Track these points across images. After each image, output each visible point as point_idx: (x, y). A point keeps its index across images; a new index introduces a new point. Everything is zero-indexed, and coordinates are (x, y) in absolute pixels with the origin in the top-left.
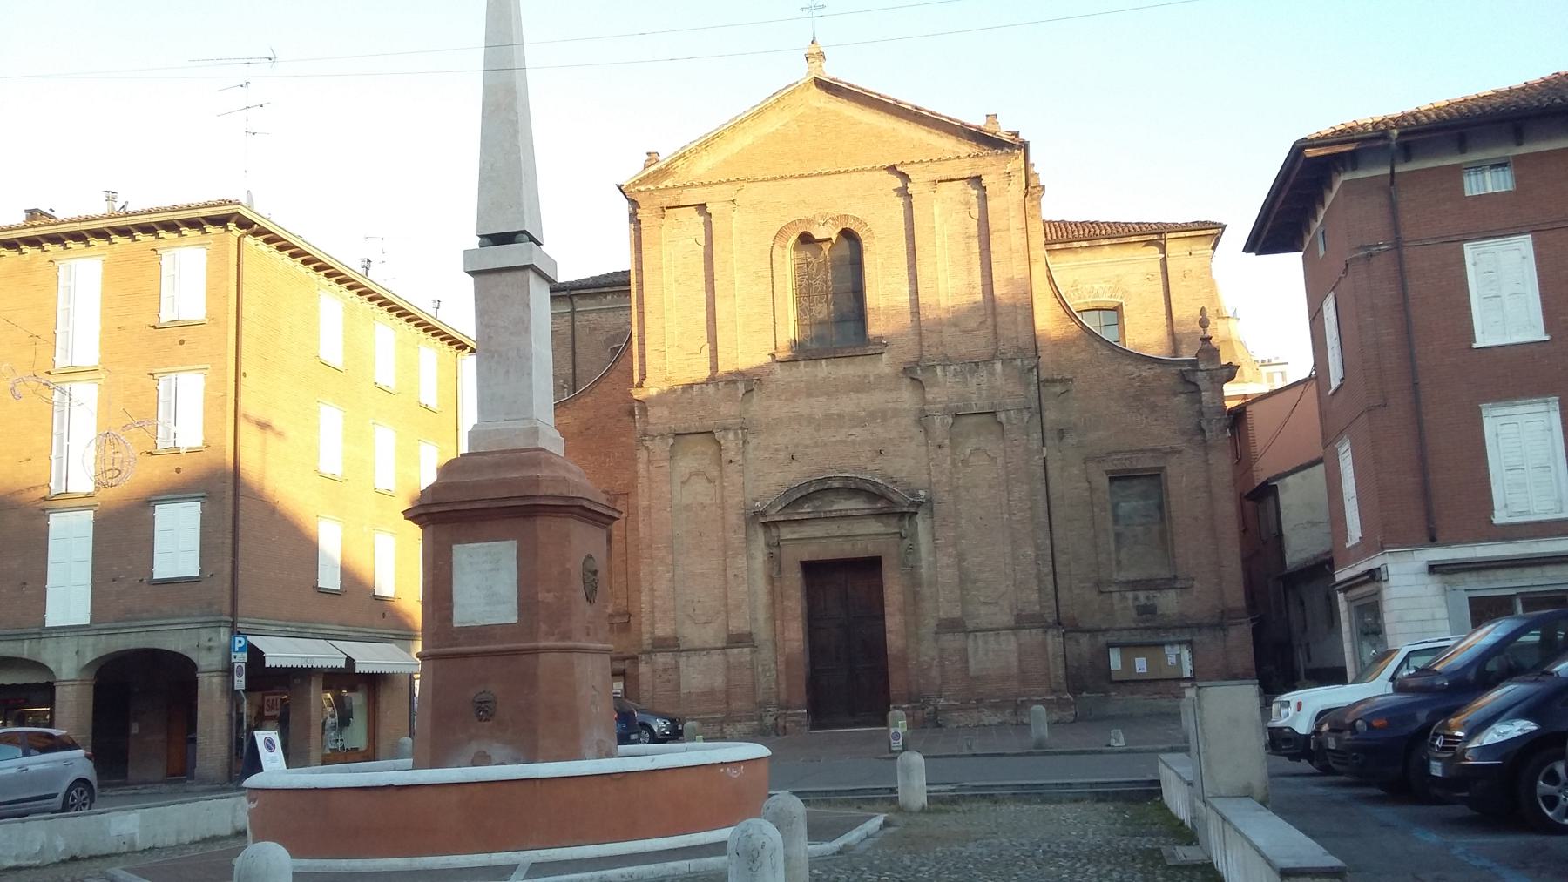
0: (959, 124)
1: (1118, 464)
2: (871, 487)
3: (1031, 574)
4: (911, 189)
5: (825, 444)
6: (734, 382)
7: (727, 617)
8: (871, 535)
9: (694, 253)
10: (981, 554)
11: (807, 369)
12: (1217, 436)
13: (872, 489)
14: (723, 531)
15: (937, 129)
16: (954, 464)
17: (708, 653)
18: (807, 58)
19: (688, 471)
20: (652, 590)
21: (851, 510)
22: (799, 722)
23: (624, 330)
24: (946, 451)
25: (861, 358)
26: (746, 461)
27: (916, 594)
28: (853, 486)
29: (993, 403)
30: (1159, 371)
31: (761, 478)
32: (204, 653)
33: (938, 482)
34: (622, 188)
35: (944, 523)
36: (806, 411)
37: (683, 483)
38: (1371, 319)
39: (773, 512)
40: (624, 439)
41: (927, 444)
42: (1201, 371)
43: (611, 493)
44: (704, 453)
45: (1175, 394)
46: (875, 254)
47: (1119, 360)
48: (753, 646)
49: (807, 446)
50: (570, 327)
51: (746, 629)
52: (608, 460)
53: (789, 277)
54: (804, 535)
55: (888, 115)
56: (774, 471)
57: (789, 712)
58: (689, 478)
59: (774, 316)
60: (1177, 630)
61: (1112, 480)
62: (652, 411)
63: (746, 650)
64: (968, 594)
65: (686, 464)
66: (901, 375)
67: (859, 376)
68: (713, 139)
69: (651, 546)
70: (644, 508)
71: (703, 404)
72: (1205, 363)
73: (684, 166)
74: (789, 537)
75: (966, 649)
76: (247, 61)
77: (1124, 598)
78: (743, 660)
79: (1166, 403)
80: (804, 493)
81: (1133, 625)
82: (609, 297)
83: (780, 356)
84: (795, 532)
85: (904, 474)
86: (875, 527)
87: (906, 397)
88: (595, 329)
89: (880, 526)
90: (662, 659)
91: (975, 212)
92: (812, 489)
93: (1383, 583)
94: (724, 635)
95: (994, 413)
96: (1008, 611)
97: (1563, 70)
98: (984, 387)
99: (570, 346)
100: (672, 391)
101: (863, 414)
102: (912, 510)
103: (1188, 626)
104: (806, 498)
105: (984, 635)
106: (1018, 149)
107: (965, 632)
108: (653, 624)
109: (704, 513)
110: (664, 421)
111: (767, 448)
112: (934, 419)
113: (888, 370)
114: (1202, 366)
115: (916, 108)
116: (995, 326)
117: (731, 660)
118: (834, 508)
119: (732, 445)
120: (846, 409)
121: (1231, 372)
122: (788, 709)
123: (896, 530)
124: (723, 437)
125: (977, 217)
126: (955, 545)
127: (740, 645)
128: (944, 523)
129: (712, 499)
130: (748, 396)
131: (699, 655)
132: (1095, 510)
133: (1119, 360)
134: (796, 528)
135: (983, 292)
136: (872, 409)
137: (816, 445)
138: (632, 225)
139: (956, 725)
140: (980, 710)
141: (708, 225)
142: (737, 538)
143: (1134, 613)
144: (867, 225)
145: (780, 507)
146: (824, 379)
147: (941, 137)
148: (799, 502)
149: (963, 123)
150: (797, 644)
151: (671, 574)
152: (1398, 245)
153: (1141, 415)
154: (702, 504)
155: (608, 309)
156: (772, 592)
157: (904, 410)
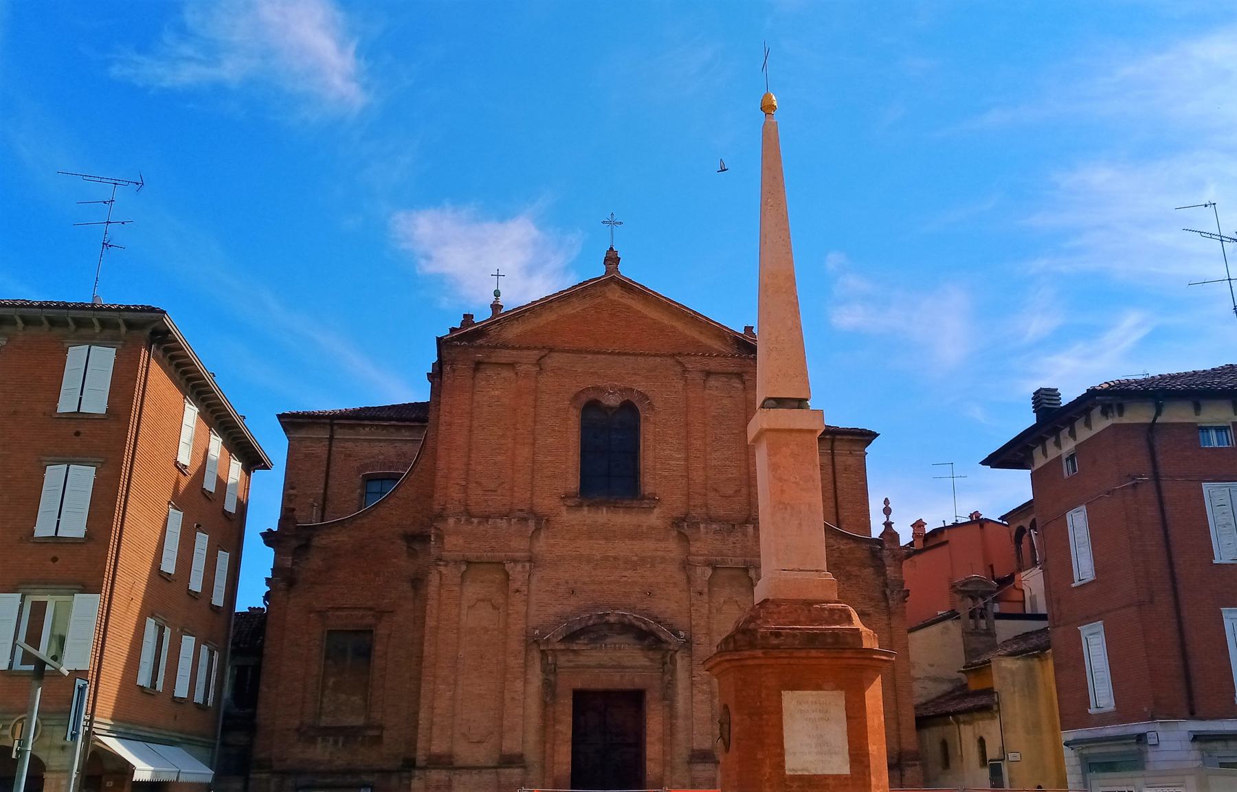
2: (643, 625)
11: (590, 515)
12: (898, 604)
20: (432, 708)
23: (377, 460)
24: (705, 597)
27: (672, 725)
32: (55, 753)
33: (697, 625)
38: (1139, 532)
40: (395, 560)
43: (377, 610)
48: (524, 767)
49: (584, 583)
50: (326, 452)
52: (377, 578)
58: (475, 604)
63: (517, 771)
65: (472, 591)
69: (435, 665)
70: (431, 628)
73: (497, 330)
76: (115, 182)
79: (859, 573)
82: (367, 429)
87: (673, 548)
88: (350, 456)
89: (646, 661)
90: (436, 776)
93: (1150, 749)
97: (1234, 363)
98: (739, 546)
99: (324, 469)
108: (430, 740)
109: (486, 637)
110: (458, 549)
113: (659, 523)
117: (503, 779)
120: (621, 554)
129: (495, 625)
142: (515, 663)
147: (711, 338)
150: (565, 767)
152: (1156, 477)
154: (485, 628)
155: (366, 439)
156: (544, 717)
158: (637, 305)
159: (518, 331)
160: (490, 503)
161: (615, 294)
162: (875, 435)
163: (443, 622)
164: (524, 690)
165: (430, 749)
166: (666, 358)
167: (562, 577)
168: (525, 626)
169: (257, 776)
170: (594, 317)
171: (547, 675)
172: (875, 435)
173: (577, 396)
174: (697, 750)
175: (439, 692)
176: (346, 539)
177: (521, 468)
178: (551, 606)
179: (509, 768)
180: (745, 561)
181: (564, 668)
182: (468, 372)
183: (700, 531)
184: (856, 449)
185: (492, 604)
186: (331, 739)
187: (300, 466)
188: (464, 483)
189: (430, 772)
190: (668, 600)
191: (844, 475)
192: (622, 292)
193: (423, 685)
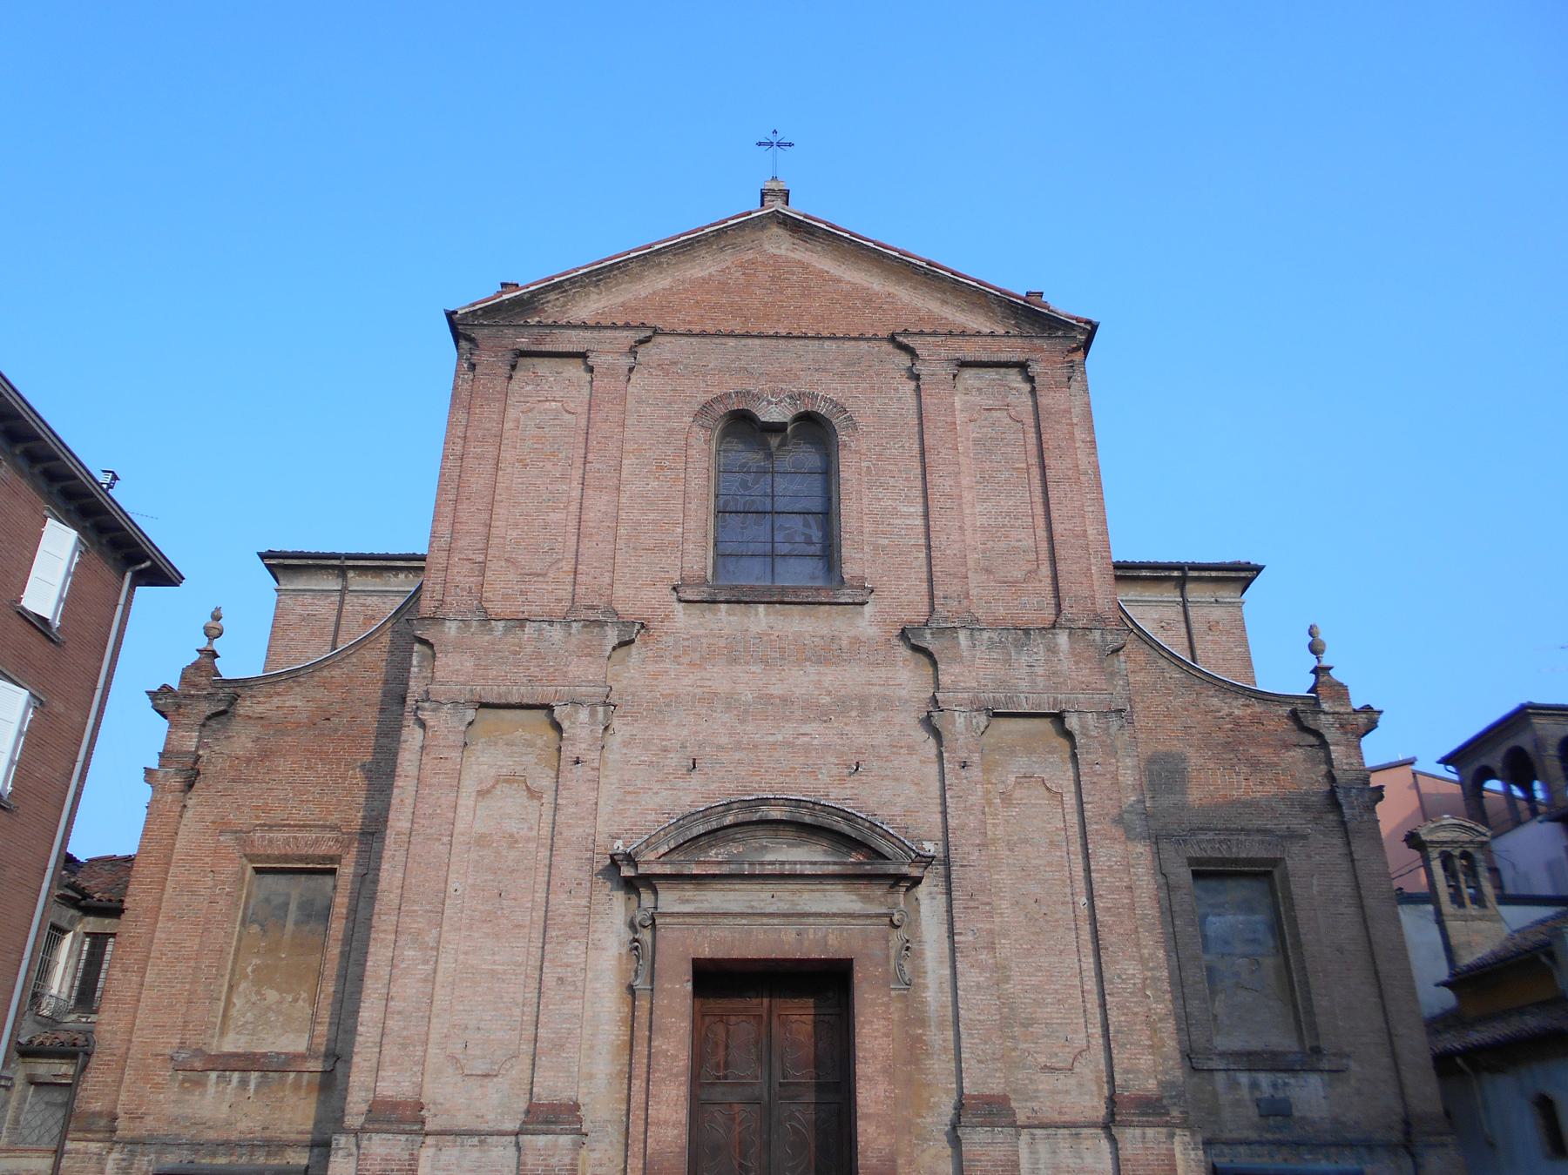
1: (1206, 848)
3: (1136, 1014)
5: (755, 746)
8: (834, 915)
9: (557, 422)
10: (1039, 968)
11: (731, 618)
13: (844, 827)
19: (493, 772)
21: (802, 863)
24: (975, 773)
28: (808, 819)
29: (1055, 699)
30: (1259, 710)
31: (629, 798)
33: (963, 827)
35: (972, 904)
36: (723, 686)
37: (482, 794)
42: (1326, 713)
44: (530, 744)
45: (1287, 746)
47: (1197, 688)
48: (579, 1132)
49: (720, 747)
51: (565, 1095)
54: (705, 907)
56: (656, 787)
58: (493, 787)
60: (1333, 1150)
61: (1196, 875)
62: (444, 660)
63: (565, 1140)
64: (1015, 1049)
65: (485, 762)
67: (823, 637)
72: (1330, 703)
74: (676, 909)
77: (1234, 1085)
80: (714, 825)
81: (1253, 1135)
84: (688, 901)
85: (896, 810)
86: (842, 899)
87: (907, 678)
90: (381, 1146)
92: (729, 820)
96: (1094, 1088)
98: (1040, 671)
99: (331, 638)
101: (826, 700)
102: (915, 872)
103: (1351, 1145)
104: (715, 835)
105: (1048, 1137)
107: (1013, 1124)
109: (513, 854)
110: (462, 679)
112: (953, 716)
113: (872, 631)
114: (1325, 706)
118: (769, 857)
119: (583, 733)
121: (1369, 718)
123: (883, 910)
128: (972, 904)
130: (622, 651)
132: (1177, 922)
133: (1197, 688)
134: (689, 891)
136: (843, 692)
137: (738, 746)
142: (567, 905)
143: (1252, 1112)
145: (665, 849)
147: (963, 310)
148: (703, 841)
153: (1238, 774)
154: (511, 836)
158: (822, 262)
159: (600, 305)
160: (531, 597)
161: (780, 245)
162: (1258, 569)
163: (422, 821)
166: (878, 343)
167: (674, 737)
168: (593, 832)
169: (80, 1145)
170: (741, 281)
171: (636, 932)
172: (1258, 569)
173: (706, 408)
175: (403, 966)
176: (299, 704)
179: (546, 1133)
181: (672, 915)
183: (959, 644)
184: (1226, 595)
185: (528, 788)
186: (236, 1076)
187: (292, 635)
188: (480, 558)
189: (370, 1139)
190: (896, 779)
191: (1208, 638)
192: (792, 240)
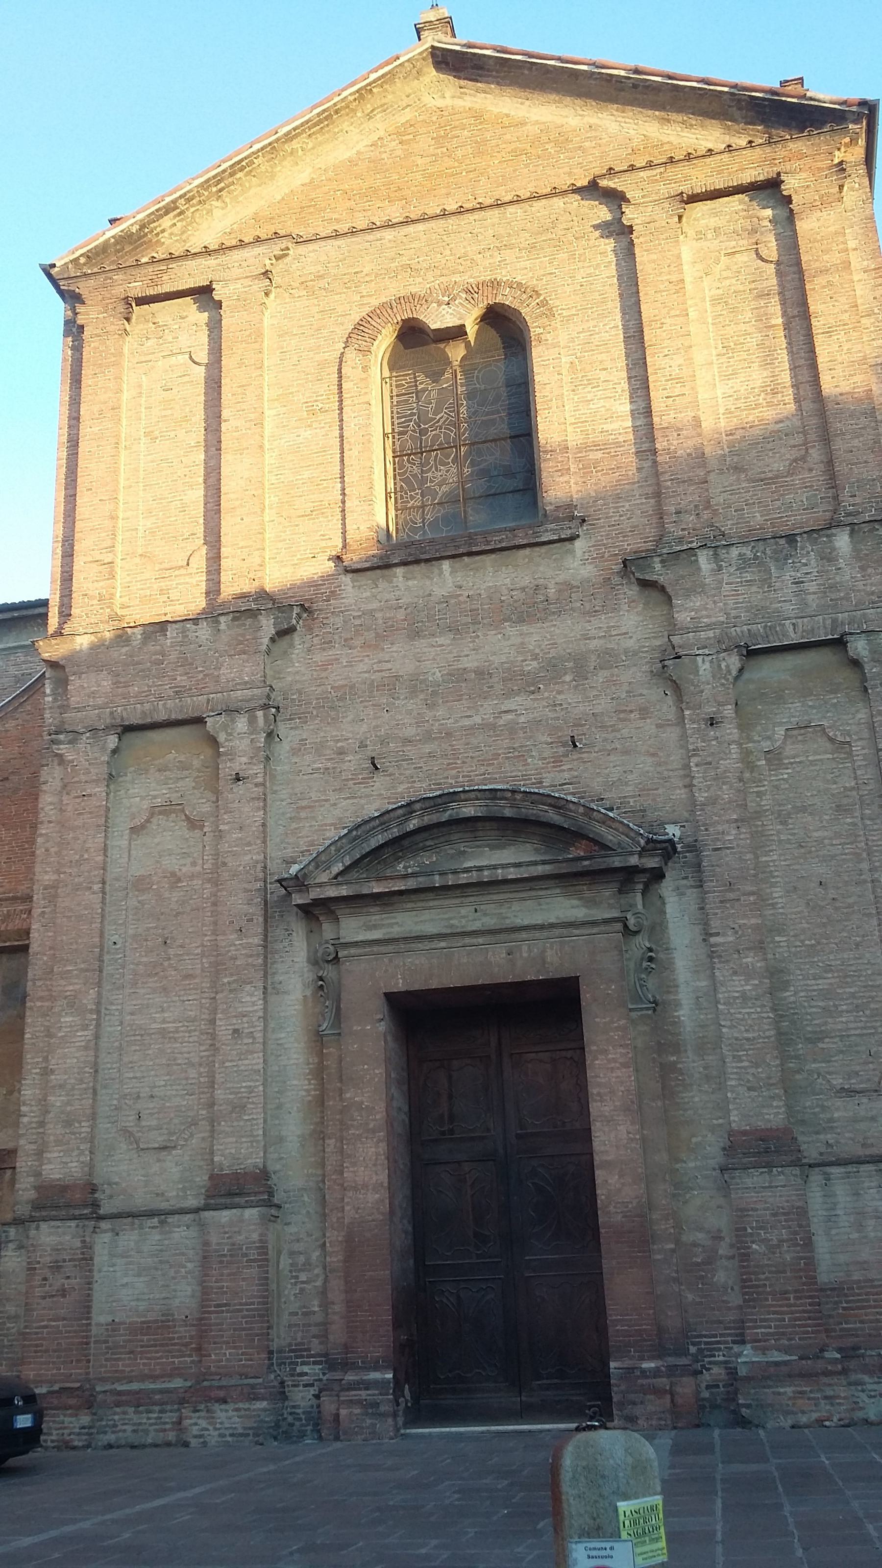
0: (726, 89)
4: (630, 215)
5: (449, 734)
6: (252, 614)
7: (212, 1131)
8: (552, 926)
9: (186, 379)
10: (828, 969)
11: (410, 583)
13: (553, 816)
14: (215, 933)
15: (679, 111)
16: (746, 757)
17: (162, 1223)
18: (418, 31)
19: (146, 805)
21: (504, 866)
22: (375, 1405)
25: (527, 551)
26: (273, 777)
27: (667, 1071)
28: (508, 813)
31: (303, 814)
34: (53, 271)
35: (731, 895)
36: (406, 668)
39: (324, 877)
41: (681, 720)
44: (184, 767)
46: (556, 345)
48: (269, 1204)
49: (407, 741)
51: (253, 1160)
53: (376, 408)
54: (396, 931)
55: (578, 101)
57: (350, 1377)
58: (148, 821)
59: (343, 482)
62: (78, 683)
63: (251, 1214)
64: (799, 1071)
66: (616, 579)
67: (523, 589)
68: (232, 175)
71: (185, 662)
73: (175, 230)
74: (360, 938)
75: (802, 1212)
78: (240, 1238)
80: (395, 832)
83: (352, 558)
84: (375, 927)
85: (629, 790)
91: (771, 248)
92: (413, 824)
94: (202, 1179)
95: (839, 643)
98: (812, 587)
100: (122, 637)
102: (652, 863)
105: (848, 1175)
106: (855, 122)
107: (796, 1163)
109: (176, 895)
110: (100, 701)
111: (319, 749)
113: (588, 571)
115: (637, 71)
116: (830, 463)
117: (214, 1239)
119: (242, 745)
122: (346, 1365)
123: (615, 914)
124: (225, 727)
125: (774, 256)
126: (760, 947)
127: (237, 1200)
128: (731, 895)
131: (141, 1227)
134: (376, 916)
135: (797, 400)
136: (553, 653)
137: (428, 737)
138: (70, 339)
139: (790, 1422)
140: (853, 1377)
141: (215, 327)
144: (538, 295)
145: (338, 867)
146: (446, 600)
149: (735, 86)
150: (373, 1197)
151: (89, 1034)
154: (173, 874)
156: (319, 1073)
157: (626, 652)
164: (265, 1009)
165: (40, 1174)
174: (745, 1133)
177: (237, 503)
178: (327, 805)
180: (834, 621)
181: (356, 944)
182: (112, 324)
193: (29, 1020)
